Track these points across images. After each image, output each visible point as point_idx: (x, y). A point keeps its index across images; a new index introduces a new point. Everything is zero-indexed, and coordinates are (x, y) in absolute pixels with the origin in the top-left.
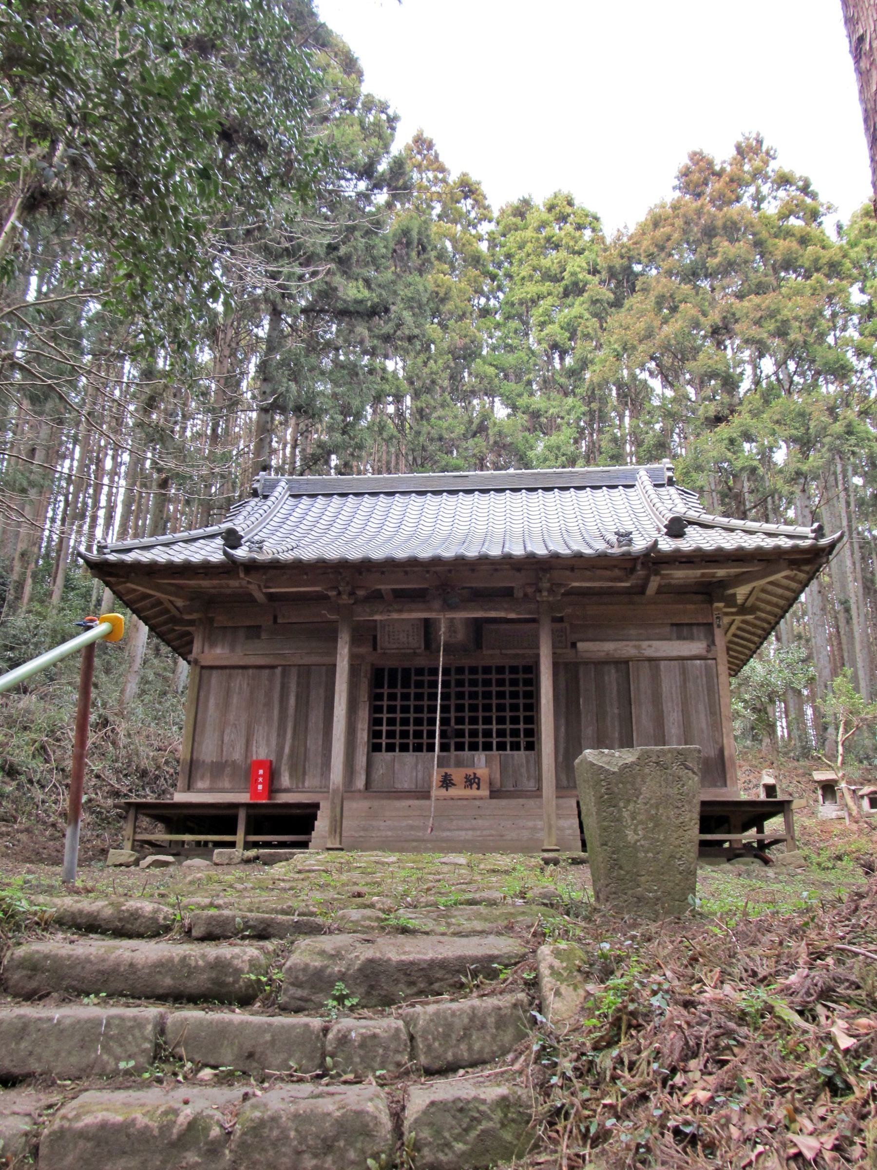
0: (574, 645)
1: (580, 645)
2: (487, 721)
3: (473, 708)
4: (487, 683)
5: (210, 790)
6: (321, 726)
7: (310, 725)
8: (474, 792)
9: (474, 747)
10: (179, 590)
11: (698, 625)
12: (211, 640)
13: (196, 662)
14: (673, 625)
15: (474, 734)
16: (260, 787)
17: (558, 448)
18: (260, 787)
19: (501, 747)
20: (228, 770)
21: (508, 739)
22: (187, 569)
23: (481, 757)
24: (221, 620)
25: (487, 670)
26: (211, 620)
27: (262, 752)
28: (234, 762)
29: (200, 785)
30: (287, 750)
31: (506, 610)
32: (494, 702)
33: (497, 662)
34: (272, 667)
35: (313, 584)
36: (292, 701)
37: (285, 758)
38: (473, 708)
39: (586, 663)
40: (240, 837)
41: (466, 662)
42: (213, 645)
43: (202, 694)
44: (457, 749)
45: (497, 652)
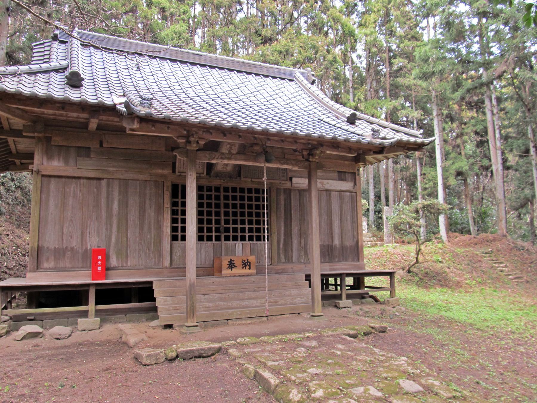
0: (291, 179)
1: (294, 180)
2: (243, 222)
3: (235, 214)
4: (242, 198)
5: (55, 269)
6: (137, 222)
7: (129, 222)
8: (247, 271)
9: (235, 239)
10: (23, 114)
11: (348, 173)
12: (49, 154)
13: (38, 172)
14: (338, 172)
15: (235, 230)
16: (99, 268)
17: (180, 34)
18: (99, 268)
19: (251, 239)
20: (69, 254)
21: (255, 234)
22: (34, 100)
23: (239, 244)
24: (57, 140)
25: (242, 190)
26: (48, 140)
27: (94, 242)
28: (72, 248)
29: (46, 265)
30: (113, 239)
31: (293, 165)
32: (247, 211)
33: (250, 186)
34: (99, 179)
35: (169, 134)
36: (116, 206)
37: (113, 245)
38: (235, 214)
39: (295, 190)
40: (91, 306)
41: (231, 185)
42: (50, 157)
43: (44, 196)
44: (225, 240)
45: (250, 180)
